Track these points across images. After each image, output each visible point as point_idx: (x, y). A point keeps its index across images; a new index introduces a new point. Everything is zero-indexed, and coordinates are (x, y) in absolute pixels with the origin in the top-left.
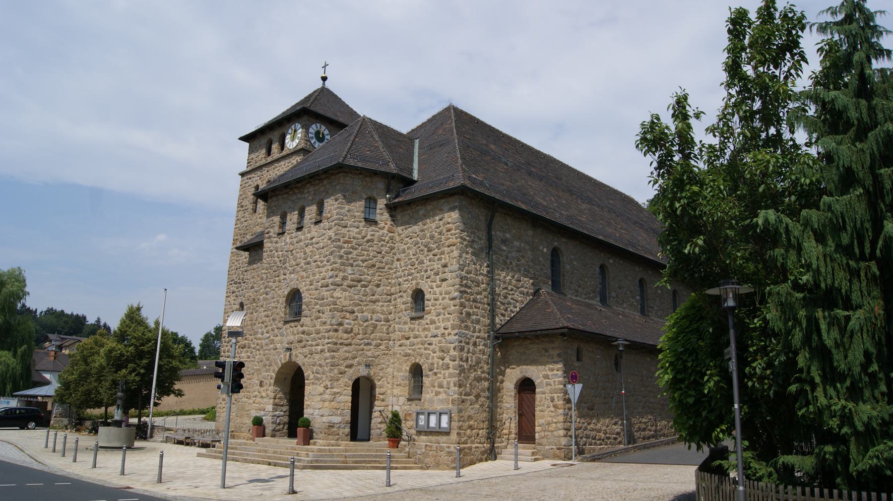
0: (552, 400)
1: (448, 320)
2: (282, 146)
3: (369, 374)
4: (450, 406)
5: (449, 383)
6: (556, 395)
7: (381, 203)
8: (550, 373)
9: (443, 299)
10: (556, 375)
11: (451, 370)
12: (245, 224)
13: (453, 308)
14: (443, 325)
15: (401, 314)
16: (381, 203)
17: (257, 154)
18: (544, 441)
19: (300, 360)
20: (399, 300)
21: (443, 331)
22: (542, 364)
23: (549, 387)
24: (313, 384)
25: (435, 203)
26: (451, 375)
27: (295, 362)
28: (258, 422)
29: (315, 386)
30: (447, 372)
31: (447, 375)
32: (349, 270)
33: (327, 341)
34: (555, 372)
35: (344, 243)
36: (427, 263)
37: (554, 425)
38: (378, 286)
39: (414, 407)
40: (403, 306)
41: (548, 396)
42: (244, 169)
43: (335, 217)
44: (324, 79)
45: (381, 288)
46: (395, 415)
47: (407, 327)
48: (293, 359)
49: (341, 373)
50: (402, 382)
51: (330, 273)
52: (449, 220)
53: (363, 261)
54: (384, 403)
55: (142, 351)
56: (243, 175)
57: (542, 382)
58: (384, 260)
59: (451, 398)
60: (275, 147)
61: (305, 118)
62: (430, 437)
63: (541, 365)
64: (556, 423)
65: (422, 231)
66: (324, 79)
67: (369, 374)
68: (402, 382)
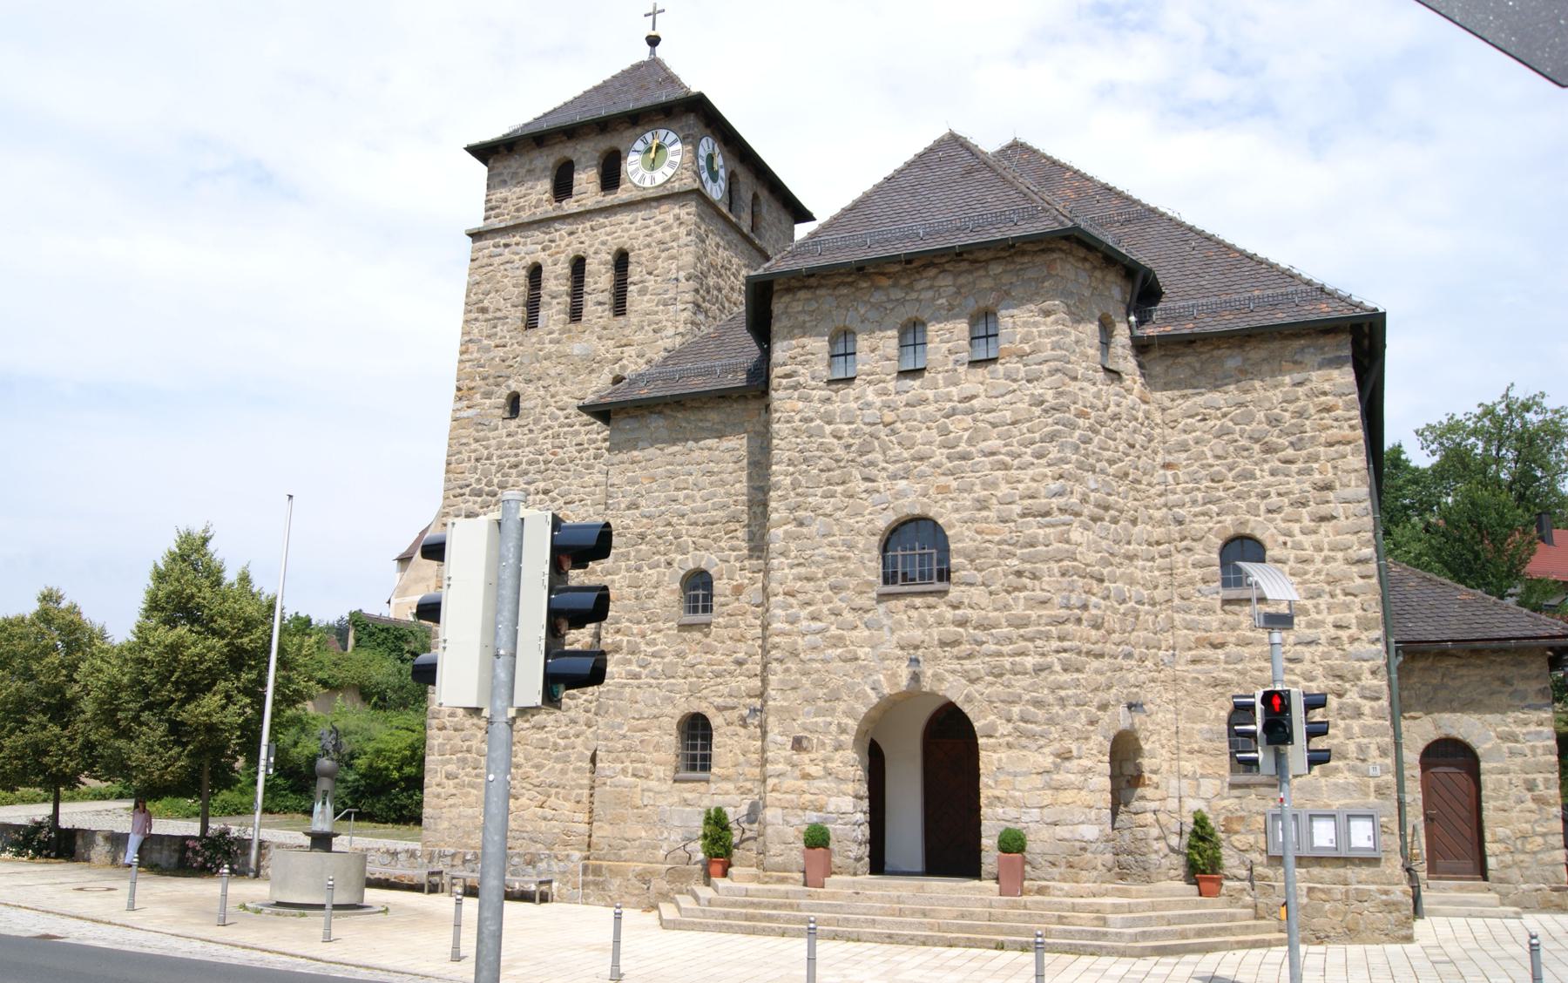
0: (1531, 786)
1: (1347, 607)
2: (611, 177)
3: (1132, 725)
4: (1372, 799)
5: (1362, 749)
6: (1539, 778)
7: (1122, 335)
8: (1517, 730)
9: (1326, 560)
10: (1538, 734)
11: (1369, 721)
12: (500, 352)
13: (1360, 581)
14: (1330, 619)
15: (1189, 589)
16: (1122, 335)
17: (518, 190)
18: (1514, 874)
19: (954, 690)
20: (1180, 557)
21: (1333, 632)
22: (1501, 709)
23: (1519, 760)
24: (1009, 746)
25: (1276, 345)
26: (1367, 731)
27: (932, 694)
28: (817, 839)
29: (1015, 753)
30: (1356, 725)
31: (1356, 730)
32: (1091, 480)
33: (1055, 644)
34: (1532, 728)
35: (1078, 416)
36: (1263, 477)
37: (1540, 840)
38: (1134, 522)
39: (1256, 803)
40: (1197, 573)
41: (1518, 778)
42: (478, 223)
43: (1048, 353)
44: (653, 41)
45: (1140, 527)
46: (1200, 821)
47: (1213, 620)
48: (927, 685)
49: (1092, 723)
50: (1206, 745)
51: (1055, 486)
52: (1327, 387)
53: (1111, 462)
54: (1159, 794)
55: (241, 651)
56: (476, 235)
57: (1497, 749)
58: (1140, 464)
59: (1372, 783)
60: (586, 180)
61: (691, 119)
62: (1316, 871)
63: (1491, 713)
64: (1544, 835)
65: (1240, 405)
66: (653, 41)
67: (1132, 725)
68: (1206, 745)
